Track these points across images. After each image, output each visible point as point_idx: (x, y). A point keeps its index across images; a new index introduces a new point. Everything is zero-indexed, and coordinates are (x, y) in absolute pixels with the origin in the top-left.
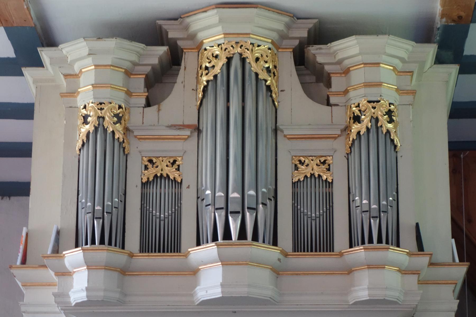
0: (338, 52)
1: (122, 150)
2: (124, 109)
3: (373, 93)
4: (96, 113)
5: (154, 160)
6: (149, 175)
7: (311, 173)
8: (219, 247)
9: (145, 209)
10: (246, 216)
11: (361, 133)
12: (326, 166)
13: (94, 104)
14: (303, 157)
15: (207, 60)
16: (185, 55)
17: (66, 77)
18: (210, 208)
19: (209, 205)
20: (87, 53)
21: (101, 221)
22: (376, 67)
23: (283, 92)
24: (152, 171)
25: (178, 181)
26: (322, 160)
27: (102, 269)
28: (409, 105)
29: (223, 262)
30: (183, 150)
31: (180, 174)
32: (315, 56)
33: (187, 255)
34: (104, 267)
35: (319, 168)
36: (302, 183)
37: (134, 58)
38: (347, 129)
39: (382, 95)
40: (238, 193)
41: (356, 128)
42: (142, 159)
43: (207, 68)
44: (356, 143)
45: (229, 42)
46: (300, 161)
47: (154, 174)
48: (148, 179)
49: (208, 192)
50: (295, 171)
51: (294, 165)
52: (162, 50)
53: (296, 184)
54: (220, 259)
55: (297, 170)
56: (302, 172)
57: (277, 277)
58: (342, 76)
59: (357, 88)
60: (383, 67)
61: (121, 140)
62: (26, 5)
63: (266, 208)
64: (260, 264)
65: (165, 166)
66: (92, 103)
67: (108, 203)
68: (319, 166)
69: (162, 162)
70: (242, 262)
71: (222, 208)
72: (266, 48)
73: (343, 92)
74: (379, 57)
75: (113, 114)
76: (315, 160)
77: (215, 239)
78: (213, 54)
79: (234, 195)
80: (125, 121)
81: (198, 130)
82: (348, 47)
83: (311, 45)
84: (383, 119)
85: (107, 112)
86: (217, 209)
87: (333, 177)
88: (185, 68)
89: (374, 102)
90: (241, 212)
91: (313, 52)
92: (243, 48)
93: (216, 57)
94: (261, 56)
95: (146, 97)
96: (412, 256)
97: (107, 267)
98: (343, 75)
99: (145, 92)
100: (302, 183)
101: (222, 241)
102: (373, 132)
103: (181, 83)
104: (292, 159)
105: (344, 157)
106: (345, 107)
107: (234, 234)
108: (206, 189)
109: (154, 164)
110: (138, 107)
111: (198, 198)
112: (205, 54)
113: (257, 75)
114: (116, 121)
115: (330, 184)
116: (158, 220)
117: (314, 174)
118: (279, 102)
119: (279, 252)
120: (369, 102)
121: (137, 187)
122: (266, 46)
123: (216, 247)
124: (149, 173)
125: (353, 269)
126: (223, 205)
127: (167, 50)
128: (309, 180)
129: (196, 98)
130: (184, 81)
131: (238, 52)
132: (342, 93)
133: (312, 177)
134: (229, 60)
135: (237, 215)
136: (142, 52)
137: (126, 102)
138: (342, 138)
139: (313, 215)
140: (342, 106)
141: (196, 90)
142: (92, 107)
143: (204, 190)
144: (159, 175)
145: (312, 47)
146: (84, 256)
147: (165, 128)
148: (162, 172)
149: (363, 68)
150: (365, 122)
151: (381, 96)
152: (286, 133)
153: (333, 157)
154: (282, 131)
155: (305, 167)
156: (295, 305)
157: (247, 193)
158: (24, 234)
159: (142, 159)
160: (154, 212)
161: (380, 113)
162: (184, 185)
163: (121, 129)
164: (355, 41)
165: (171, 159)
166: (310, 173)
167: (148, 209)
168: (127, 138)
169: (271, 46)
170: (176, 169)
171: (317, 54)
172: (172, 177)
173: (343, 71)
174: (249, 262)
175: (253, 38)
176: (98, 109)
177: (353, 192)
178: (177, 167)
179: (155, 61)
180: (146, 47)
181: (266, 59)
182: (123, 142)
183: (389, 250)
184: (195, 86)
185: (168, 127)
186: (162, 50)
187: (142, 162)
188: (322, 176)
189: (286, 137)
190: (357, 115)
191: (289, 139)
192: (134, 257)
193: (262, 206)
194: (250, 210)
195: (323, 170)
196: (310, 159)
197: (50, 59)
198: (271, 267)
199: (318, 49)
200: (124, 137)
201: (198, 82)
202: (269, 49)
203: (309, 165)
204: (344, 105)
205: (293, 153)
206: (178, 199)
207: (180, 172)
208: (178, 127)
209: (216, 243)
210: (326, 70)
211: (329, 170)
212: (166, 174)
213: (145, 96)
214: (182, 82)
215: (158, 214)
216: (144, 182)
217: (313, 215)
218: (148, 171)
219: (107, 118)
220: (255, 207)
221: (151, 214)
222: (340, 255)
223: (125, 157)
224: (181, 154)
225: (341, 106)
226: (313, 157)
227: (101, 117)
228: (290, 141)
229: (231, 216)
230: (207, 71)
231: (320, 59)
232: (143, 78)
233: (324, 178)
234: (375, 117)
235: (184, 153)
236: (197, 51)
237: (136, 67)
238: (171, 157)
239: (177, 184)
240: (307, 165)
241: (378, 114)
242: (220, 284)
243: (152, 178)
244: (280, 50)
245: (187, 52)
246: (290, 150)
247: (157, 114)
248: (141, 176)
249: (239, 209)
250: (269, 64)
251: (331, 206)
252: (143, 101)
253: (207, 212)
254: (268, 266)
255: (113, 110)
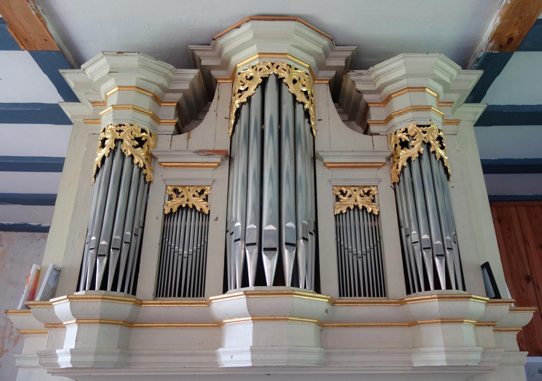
0: (379, 77)
1: (142, 177)
2: (149, 134)
3: (422, 117)
4: (114, 135)
5: (180, 190)
6: (172, 206)
7: (354, 205)
8: (249, 297)
9: (166, 244)
10: (283, 254)
11: (413, 159)
12: (371, 197)
13: (113, 126)
14: (345, 187)
15: (241, 83)
16: (219, 86)
17: (94, 104)
18: (240, 244)
19: (239, 240)
20: (108, 72)
21: (105, 259)
22: (422, 92)
23: (320, 121)
24: (177, 202)
25: (205, 213)
26: (366, 190)
27: (96, 322)
28: (454, 135)
29: (253, 317)
30: (212, 178)
31: (207, 205)
32: (355, 84)
33: (209, 303)
34: (98, 321)
35: (363, 199)
36: (344, 216)
37: (162, 80)
38: (392, 158)
39: (431, 119)
40: (274, 225)
41: (405, 154)
42: (166, 188)
43: (240, 91)
44: (407, 171)
45: (264, 62)
46: (342, 192)
47: (179, 205)
48: (171, 210)
49: (238, 224)
50: (336, 202)
51: (335, 196)
52: (192, 73)
53: (338, 217)
54: (249, 313)
55: (338, 201)
56: (344, 203)
57: (322, 330)
58: (381, 107)
59: (402, 113)
60: (429, 93)
61: (142, 165)
62: (34, 11)
63: (308, 243)
64: (303, 318)
65: (192, 195)
66: (111, 125)
67: (116, 237)
68: (362, 197)
69: (188, 192)
70: (280, 316)
71: (254, 244)
72: (303, 72)
73: (384, 121)
74: (426, 80)
75: (134, 137)
76: (358, 190)
77: (245, 283)
78: (247, 77)
79: (269, 227)
80: (148, 146)
81: (230, 157)
82: (393, 70)
83: (352, 70)
84: (436, 146)
85: (126, 134)
86: (248, 245)
87: (379, 209)
88: (219, 97)
89: (424, 126)
90: (278, 249)
91: (353, 78)
92: (279, 68)
93: (251, 78)
94: (299, 79)
95: (175, 124)
96: (489, 304)
97: (103, 320)
98: (382, 105)
99: (174, 119)
100: (344, 216)
101: (253, 287)
102: (425, 157)
103: (214, 111)
104: (334, 189)
105: (390, 187)
106: (386, 136)
107: (269, 277)
108: (236, 221)
109: (179, 193)
110: (167, 134)
111: (227, 231)
112: (239, 77)
113: (294, 96)
114: (137, 145)
115: (375, 217)
116: (180, 257)
117: (357, 205)
118: (317, 131)
119: (327, 302)
120: (419, 126)
121: (158, 219)
122: (303, 71)
123: (245, 296)
124: (174, 204)
125: (418, 322)
126: (255, 240)
127: (198, 73)
128: (352, 212)
129: (228, 126)
130: (217, 110)
131: (273, 73)
132: (383, 122)
133: (355, 210)
134: (263, 85)
135: (273, 252)
136: (171, 75)
137: (151, 126)
138: (386, 168)
139: (359, 252)
140: (383, 135)
141: (229, 119)
142: (111, 129)
143: (233, 221)
144: (184, 206)
145: (352, 72)
146: (71, 307)
147: (192, 154)
148: (188, 203)
149: (408, 93)
150: (417, 147)
151: (430, 120)
152: (325, 160)
153: (377, 188)
154: (321, 159)
155: (347, 197)
156: (345, 367)
157: (285, 225)
158: (33, 272)
159: (166, 189)
160: (176, 248)
161: (432, 139)
162: (212, 217)
163: (143, 154)
164: (402, 61)
165: (198, 189)
166: (353, 205)
167: (169, 244)
168: (150, 164)
169: (308, 71)
170: (204, 199)
171: (357, 81)
172: (198, 209)
173: (382, 101)
174: (289, 317)
175: (290, 60)
176: (117, 131)
177: (405, 225)
178: (205, 197)
179: (186, 86)
180: (175, 69)
181: (304, 83)
182: (144, 166)
183: (471, 299)
184: (229, 115)
185: (195, 152)
186: (192, 73)
187: (166, 191)
188: (367, 208)
189: (326, 166)
190: (405, 140)
191: (329, 168)
192: (142, 305)
193: (303, 241)
194: (288, 246)
195: (367, 201)
196: (353, 190)
197: (75, 84)
198: (317, 321)
199: (358, 75)
200: (146, 163)
201: (232, 103)
202: (307, 74)
203: (352, 196)
204: (385, 134)
205: (334, 183)
206: (204, 233)
207: (207, 202)
208: (207, 153)
209: (245, 292)
210: (364, 99)
211: (373, 201)
212: (192, 204)
213: (174, 123)
214: (215, 111)
215: (181, 250)
216: (167, 214)
217: (359, 252)
218: (172, 201)
219: (126, 142)
220: (294, 242)
221: (172, 250)
222: (399, 303)
223: (147, 186)
224: (210, 183)
225: (382, 135)
226: (356, 188)
227: (119, 140)
228: (330, 170)
229: (265, 254)
230: (240, 94)
231: (360, 87)
232: (173, 106)
233: (369, 210)
234: (427, 142)
235: (213, 182)
236: (231, 81)
237: (166, 94)
238: (198, 186)
239: (205, 216)
240: (350, 196)
241: (430, 139)
242: (249, 348)
243: (176, 209)
244: (316, 82)
245: (221, 82)
246: (330, 180)
247: (186, 142)
248: (164, 206)
249: (275, 245)
250: (307, 89)
251: (378, 241)
252: (172, 128)
253: (236, 248)
254: (314, 320)
255: (134, 133)
